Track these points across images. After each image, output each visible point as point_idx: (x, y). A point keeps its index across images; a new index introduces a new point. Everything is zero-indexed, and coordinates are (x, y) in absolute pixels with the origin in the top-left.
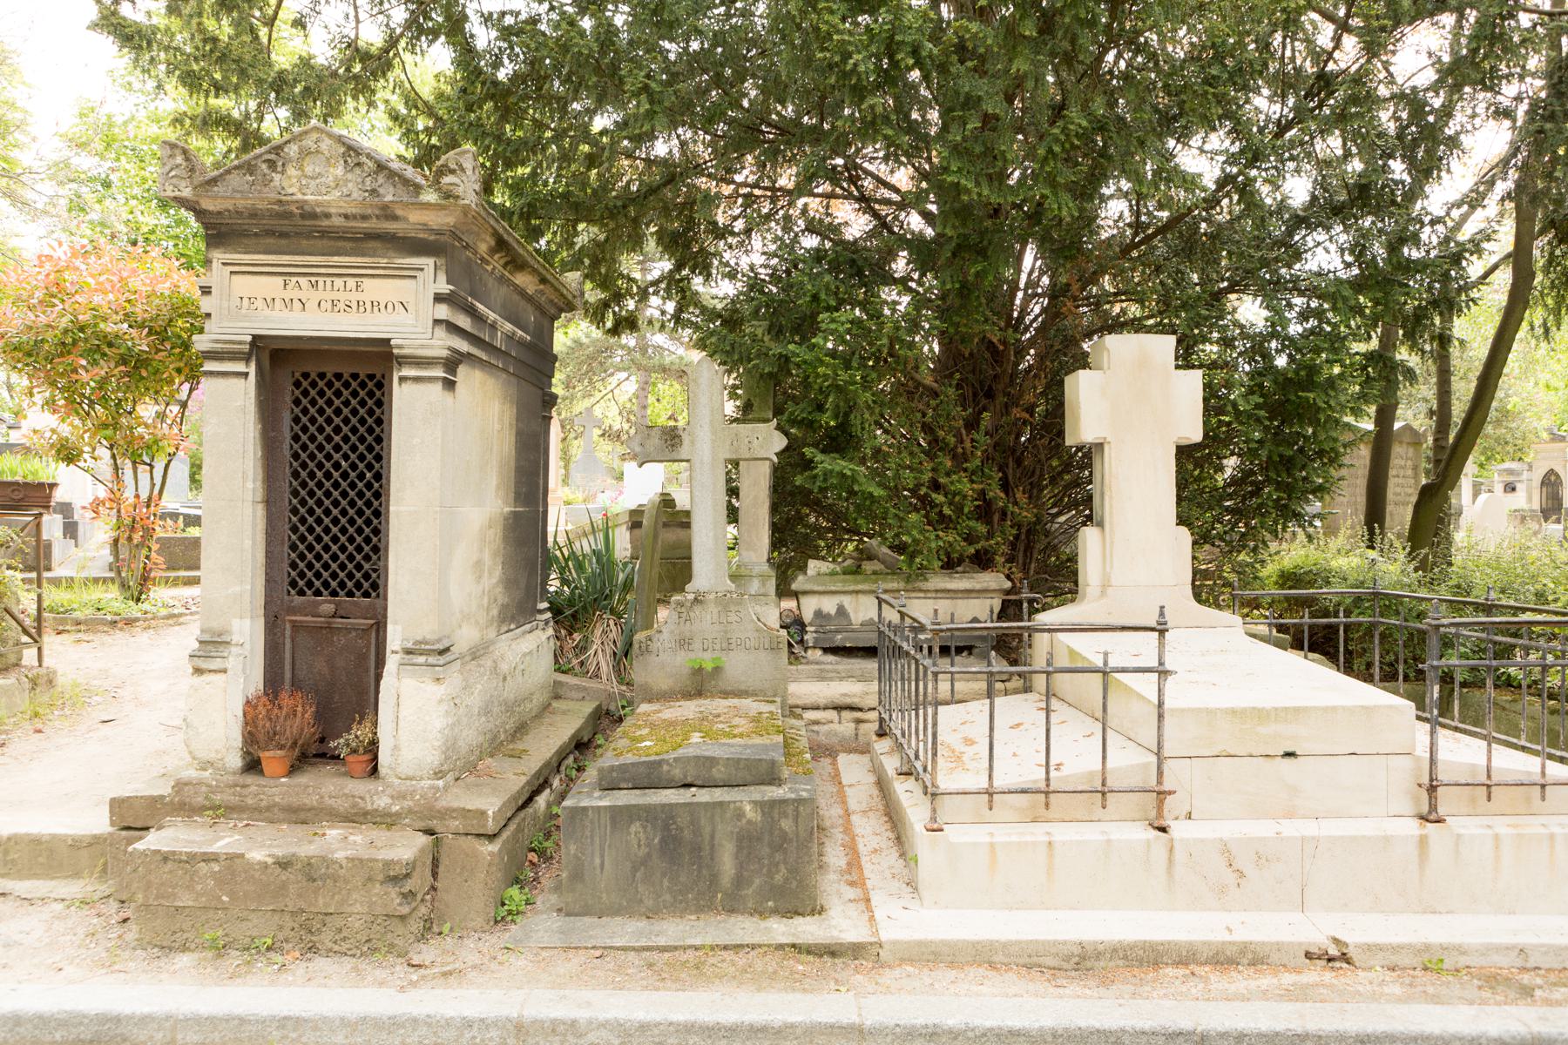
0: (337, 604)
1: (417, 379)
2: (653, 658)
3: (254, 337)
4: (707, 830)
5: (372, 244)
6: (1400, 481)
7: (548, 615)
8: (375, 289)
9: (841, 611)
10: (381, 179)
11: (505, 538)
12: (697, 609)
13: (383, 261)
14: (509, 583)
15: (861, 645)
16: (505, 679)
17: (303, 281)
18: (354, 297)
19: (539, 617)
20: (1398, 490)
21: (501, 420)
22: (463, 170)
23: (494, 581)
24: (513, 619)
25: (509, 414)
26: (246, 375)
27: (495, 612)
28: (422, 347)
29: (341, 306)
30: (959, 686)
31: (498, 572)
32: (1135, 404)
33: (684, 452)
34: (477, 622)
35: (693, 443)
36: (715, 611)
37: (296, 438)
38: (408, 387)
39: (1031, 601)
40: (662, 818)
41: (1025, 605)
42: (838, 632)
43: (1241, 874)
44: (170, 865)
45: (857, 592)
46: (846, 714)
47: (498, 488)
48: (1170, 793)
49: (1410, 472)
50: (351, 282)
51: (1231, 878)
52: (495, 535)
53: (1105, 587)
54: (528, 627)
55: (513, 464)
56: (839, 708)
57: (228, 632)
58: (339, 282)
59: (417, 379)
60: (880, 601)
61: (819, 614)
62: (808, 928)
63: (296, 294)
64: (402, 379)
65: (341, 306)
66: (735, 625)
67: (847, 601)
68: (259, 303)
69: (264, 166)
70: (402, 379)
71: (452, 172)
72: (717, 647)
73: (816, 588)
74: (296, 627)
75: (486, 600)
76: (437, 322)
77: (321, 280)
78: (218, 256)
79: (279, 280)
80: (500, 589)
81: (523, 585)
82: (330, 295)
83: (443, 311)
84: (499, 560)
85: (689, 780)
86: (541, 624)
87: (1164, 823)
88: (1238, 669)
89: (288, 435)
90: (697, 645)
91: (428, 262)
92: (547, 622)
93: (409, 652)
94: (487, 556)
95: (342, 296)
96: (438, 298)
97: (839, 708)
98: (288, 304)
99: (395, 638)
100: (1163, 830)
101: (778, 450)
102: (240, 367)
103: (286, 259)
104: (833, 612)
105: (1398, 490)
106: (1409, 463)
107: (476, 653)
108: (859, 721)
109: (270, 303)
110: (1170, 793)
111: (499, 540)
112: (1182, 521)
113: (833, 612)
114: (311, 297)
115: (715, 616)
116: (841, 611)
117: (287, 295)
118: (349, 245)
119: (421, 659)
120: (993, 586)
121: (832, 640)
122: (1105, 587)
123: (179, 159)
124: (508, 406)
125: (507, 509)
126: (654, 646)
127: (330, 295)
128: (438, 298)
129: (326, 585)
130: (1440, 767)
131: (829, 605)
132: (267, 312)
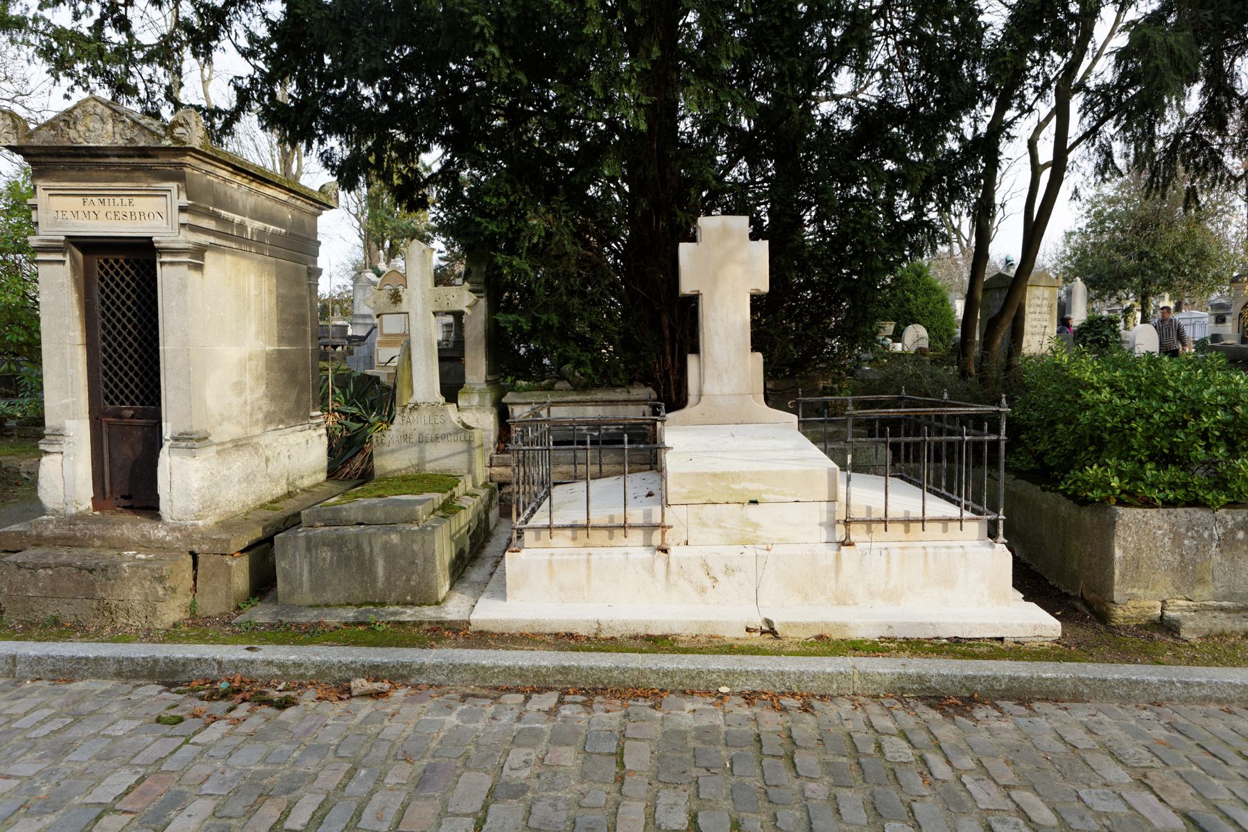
0: (135, 410)
1: (172, 263)
3: (67, 237)
4: (367, 550)
5: (138, 174)
6: (1037, 316)
8: (142, 204)
10: (136, 131)
12: (415, 414)
13: (144, 186)
16: (267, 460)
17: (95, 199)
18: (128, 209)
20: (1034, 323)
22: (188, 123)
26: (63, 262)
28: (173, 242)
29: (120, 215)
30: (604, 468)
31: (262, 389)
32: (726, 267)
33: (404, 307)
35: (409, 301)
37: (103, 303)
38: (166, 269)
43: (716, 580)
44: (1107, 790)
47: (258, 333)
48: (669, 527)
49: (1045, 309)
50: (126, 200)
51: (708, 582)
52: (260, 365)
53: (700, 395)
54: (299, 428)
55: (274, 317)
57: (64, 429)
58: (118, 200)
59: (172, 263)
62: (428, 612)
63: (91, 208)
64: (162, 263)
65: (120, 215)
68: (69, 215)
69: (62, 124)
70: (162, 263)
71: (181, 125)
73: (518, 401)
74: (109, 424)
75: (248, 408)
76: (183, 225)
77: (106, 199)
78: (41, 184)
79: (80, 199)
82: (113, 209)
83: (185, 218)
85: (360, 520)
87: (665, 547)
88: (780, 449)
89: (98, 303)
91: (173, 185)
92: (318, 425)
93: (176, 439)
94: (248, 380)
95: (121, 209)
96: (182, 209)
98: (87, 215)
99: (168, 430)
100: (665, 551)
102: (59, 257)
103: (90, 185)
105: (1034, 323)
106: (1045, 302)
107: (238, 444)
109: (75, 214)
110: (669, 527)
112: (758, 343)
114: (102, 210)
117: (86, 209)
118: (122, 175)
119: (184, 444)
122: (700, 395)
123: (8, 121)
125: (269, 348)
126: (386, 440)
127: (113, 209)
128: (182, 209)
129: (127, 398)
130: (852, 509)
132: (74, 221)
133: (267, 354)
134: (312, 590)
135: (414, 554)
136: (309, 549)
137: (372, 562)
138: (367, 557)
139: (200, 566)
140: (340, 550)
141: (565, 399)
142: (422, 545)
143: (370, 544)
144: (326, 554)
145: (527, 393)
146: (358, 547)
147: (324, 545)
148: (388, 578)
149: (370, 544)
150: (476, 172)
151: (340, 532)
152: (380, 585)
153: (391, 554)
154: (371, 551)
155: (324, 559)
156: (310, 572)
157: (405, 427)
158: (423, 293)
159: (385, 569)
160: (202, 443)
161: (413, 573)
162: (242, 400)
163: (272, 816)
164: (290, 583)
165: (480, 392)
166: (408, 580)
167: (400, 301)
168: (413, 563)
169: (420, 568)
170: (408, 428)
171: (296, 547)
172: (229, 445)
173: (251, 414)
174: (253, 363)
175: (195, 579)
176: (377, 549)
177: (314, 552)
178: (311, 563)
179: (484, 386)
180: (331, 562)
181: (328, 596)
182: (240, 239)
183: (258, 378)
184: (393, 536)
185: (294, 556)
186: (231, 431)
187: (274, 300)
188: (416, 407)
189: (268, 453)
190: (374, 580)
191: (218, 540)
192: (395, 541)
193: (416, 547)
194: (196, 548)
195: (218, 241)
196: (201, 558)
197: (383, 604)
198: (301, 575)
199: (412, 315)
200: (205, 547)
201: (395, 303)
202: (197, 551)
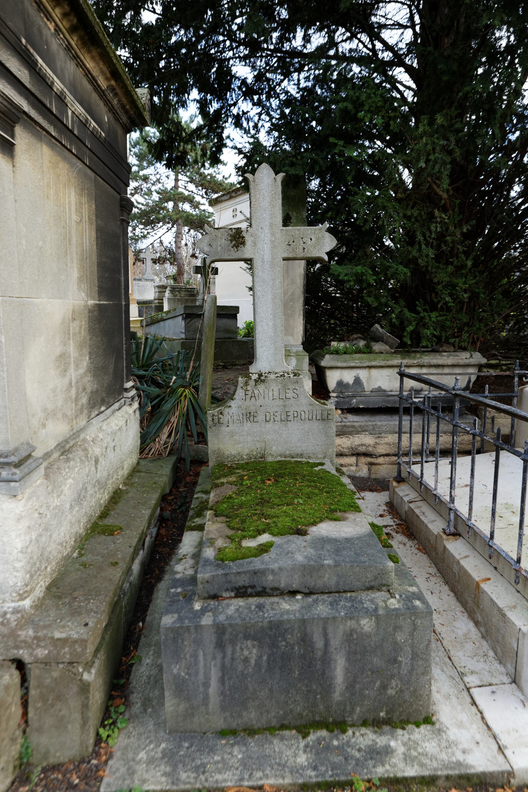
2: (224, 429)
4: (319, 644)
7: (133, 392)
9: (357, 380)
11: (91, 330)
12: (261, 387)
14: (97, 371)
15: (371, 406)
16: (97, 461)
19: (126, 395)
21: (79, 211)
23: (81, 371)
24: (103, 402)
25: (88, 209)
27: (84, 400)
31: (86, 361)
33: (247, 251)
34: (65, 415)
35: (255, 244)
36: (276, 389)
39: (521, 377)
40: (271, 635)
41: (516, 379)
42: (354, 396)
45: (370, 367)
46: (363, 460)
47: (80, 280)
52: (80, 328)
54: (117, 405)
56: (358, 455)
60: (402, 375)
61: (340, 384)
66: (292, 401)
67: (363, 374)
72: (278, 419)
73: (339, 364)
75: (73, 391)
80: (88, 378)
81: (111, 370)
84: (86, 351)
85: (295, 587)
86: (128, 400)
90: (261, 417)
92: (133, 398)
94: (72, 350)
97: (358, 455)
101: (328, 250)
104: (351, 382)
107: (65, 449)
108: (371, 464)
111: (84, 333)
113: (351, 382)
115: (276, 394)
116: (357, 380)
120: (472, 361)
121: (349, 403)
124: (84, 200)
125: (91, 302)
126: (224, 419)
131: (348, 377)
133: (90, 311)
134: (223, 709)
135: (397, 648)
136: (220, 645)
137: (326, 660)
138: (319, 654)
139: (32, 683)
140: (274, 645)
141: (390, 363)
142: (412, 634)
143: (325, 635)
144: (250, 651)
145: (347, 356)
146: (305, 640)
147: (247, 637)
148: (350, 686)
149: (325, 635)
150: (132, 160)
151: (269, 614)
152: (337, 696)
153: (357, 648)
154: (327, 644)
155: (246, 660)
156: (222, 681)
157: (248, 403)
158: (273, 234)
159: (347, 670)
160: (25, 468)
161: (392, 676)
162: (66, 381)
163: (7, 688)
164: (188, 699)
165: (297, 355)
166: (384, 687)
167: (243, 243)
168: (395, 661)
169: (404, 670)
170: (252, 405)
171: (198, 642)
172: (56, 455)
173: (77, 400)
174: (77, 323)
175: (25, 704)
176: (335, 642)
177: (229, 650)
178: (223, 667)
179: (301, 348)
180: (258, 664)
181: (251, 716)
182: (57, 121)
183: (81, 346)
184: (364, 622)
185: (195, 656)
186: (55, 431)
187: (94, 234)
188: (261, 379)
189: (97, 451)
190: (327, 688)
191: (65, 641)
192: (367, 629)
193: (400, 637)
194: (24, 654)
195: (33, 113)
196: (34, 672)
197: (339, 726)
198: (206, 685)
199: (257, 263)
200: (41, 653)
201: (237, 246)
202: (27, 658)
